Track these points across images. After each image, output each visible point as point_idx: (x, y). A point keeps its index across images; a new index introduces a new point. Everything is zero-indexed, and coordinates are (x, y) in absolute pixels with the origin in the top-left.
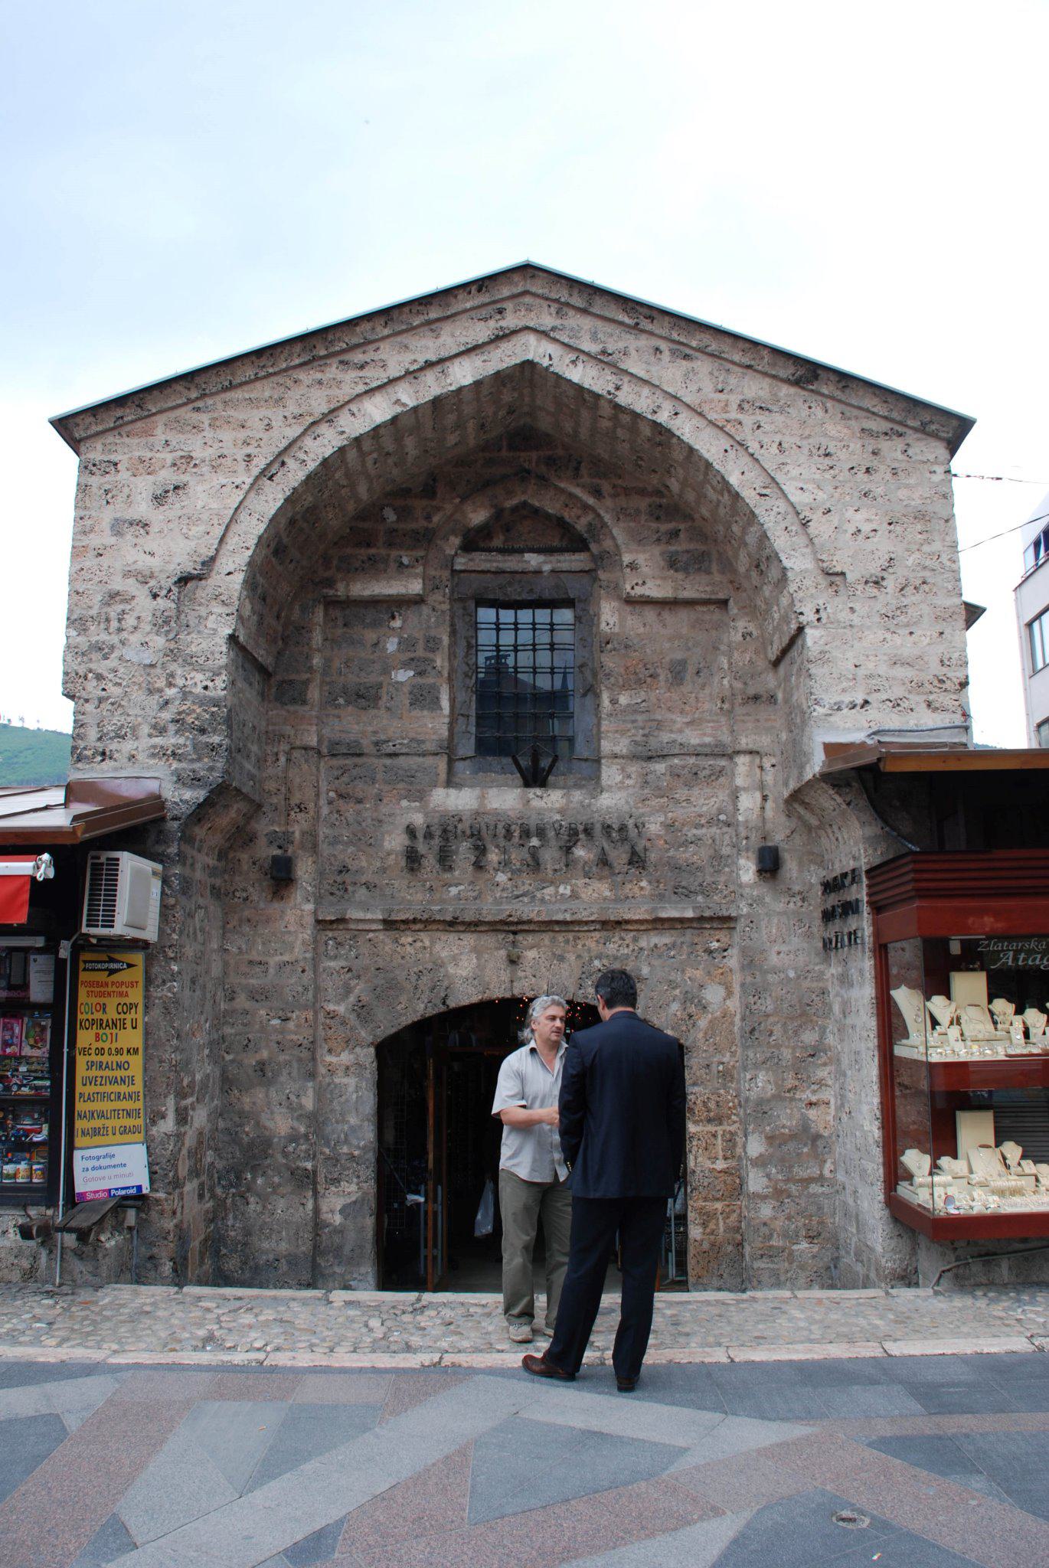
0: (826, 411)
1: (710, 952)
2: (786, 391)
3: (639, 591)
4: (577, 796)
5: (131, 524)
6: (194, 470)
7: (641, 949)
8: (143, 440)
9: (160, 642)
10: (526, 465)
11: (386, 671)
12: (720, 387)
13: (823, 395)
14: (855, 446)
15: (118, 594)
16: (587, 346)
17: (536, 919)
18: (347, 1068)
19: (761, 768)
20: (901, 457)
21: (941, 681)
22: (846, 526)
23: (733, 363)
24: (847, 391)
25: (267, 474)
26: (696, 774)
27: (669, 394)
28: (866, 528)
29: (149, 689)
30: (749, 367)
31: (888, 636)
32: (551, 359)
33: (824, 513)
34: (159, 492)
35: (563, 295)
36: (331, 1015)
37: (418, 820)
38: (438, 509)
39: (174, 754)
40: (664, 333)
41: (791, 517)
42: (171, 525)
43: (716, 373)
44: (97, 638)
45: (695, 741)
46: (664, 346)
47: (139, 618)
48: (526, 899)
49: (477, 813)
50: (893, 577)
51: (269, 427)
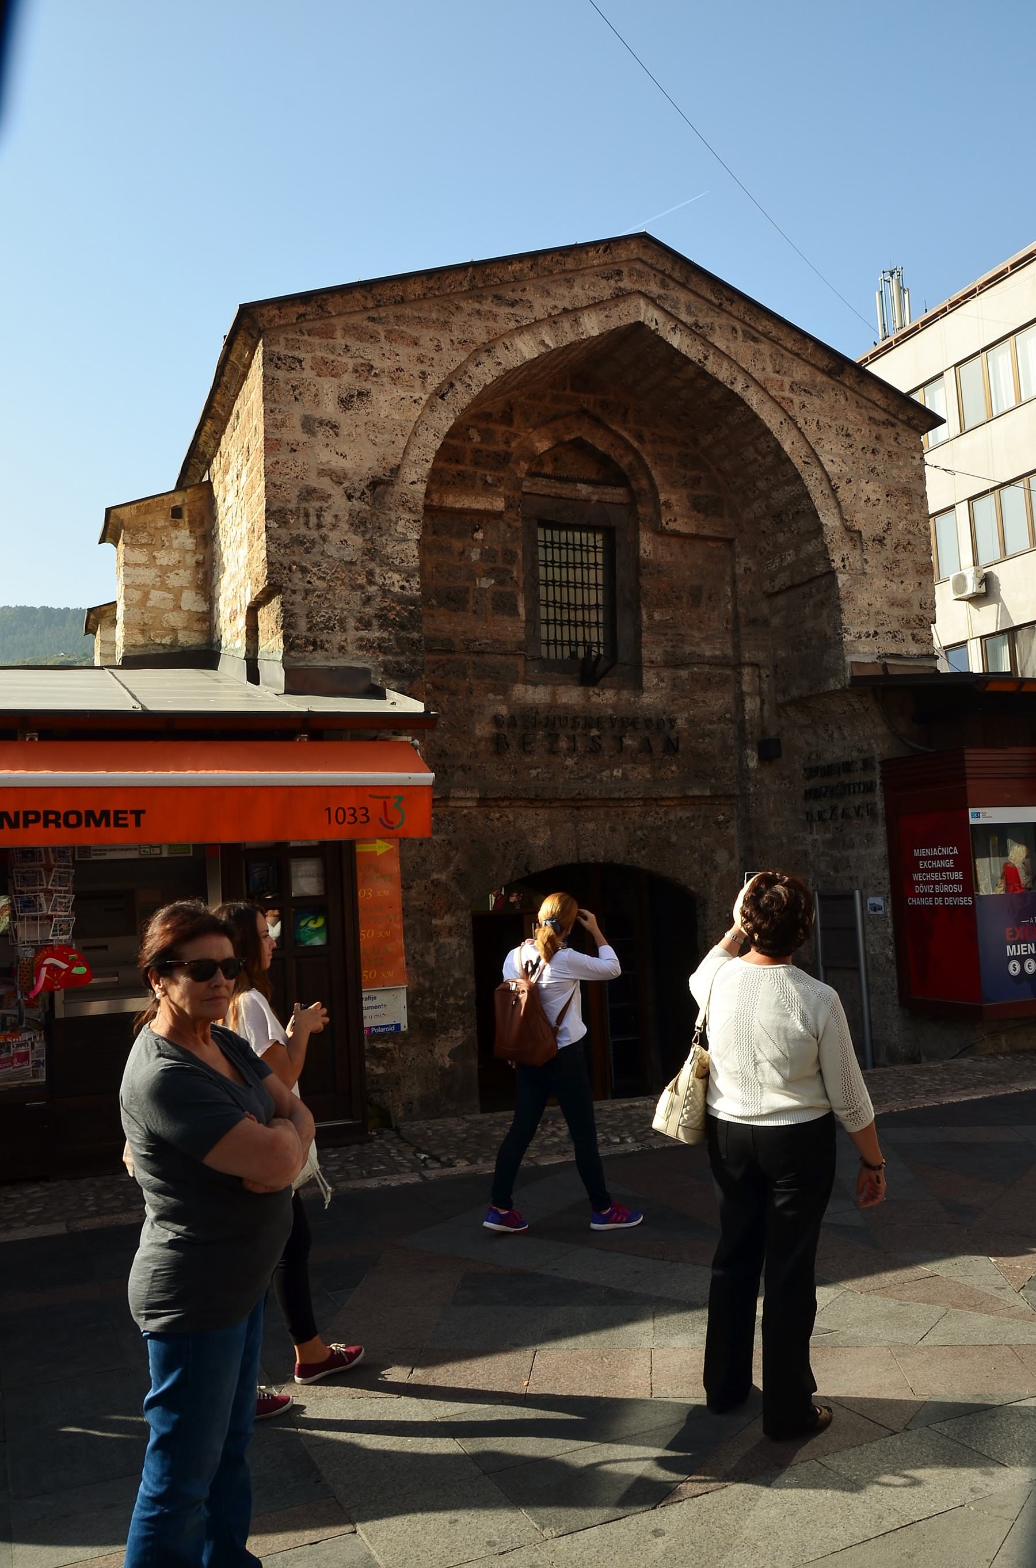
0: (847, 400)
1: (718, 823)
2: (821, 378)
3: (672, 526)
4: (625, 694)
5: (321, 424)
6: (375, 379)
7: (670, 821)
8: (325, 342)
9: (357, 541)
10: (585, 406)
11: (471, 578)
12: (777, 369)
13: (845, 385)
14: (865, 430)
15: (314, 490)
16: (684, 317)
17: (598, 797)
18: (451, 929)
19: (759, 676)
20: (894, 443)
21: (921, 620)
22: (861, 495)
23: (786, 349)
24: (862, 385)
25: (440, 394)
26: (709, 680)
27: (743, 369)
28: (873, 497)
29: (351, 586)
30: (797, 355)
31: (888, 583)
32: (657, 324)
33: (847, 483)
34: (344, 396)
35: (667, 266)
36: (436, 883)
37: (503, 710)
38: (516, 435)
39: (380, 646)
40: (740, 315)
41: (825, 484)
42: (358, 430)
43: (775, 357)
44: (298, 532)
45: (708, 653)
46: (738, 326)
47: (336, 516)
48: (589, 781)
50: (890, 537)
51: (438, 348)
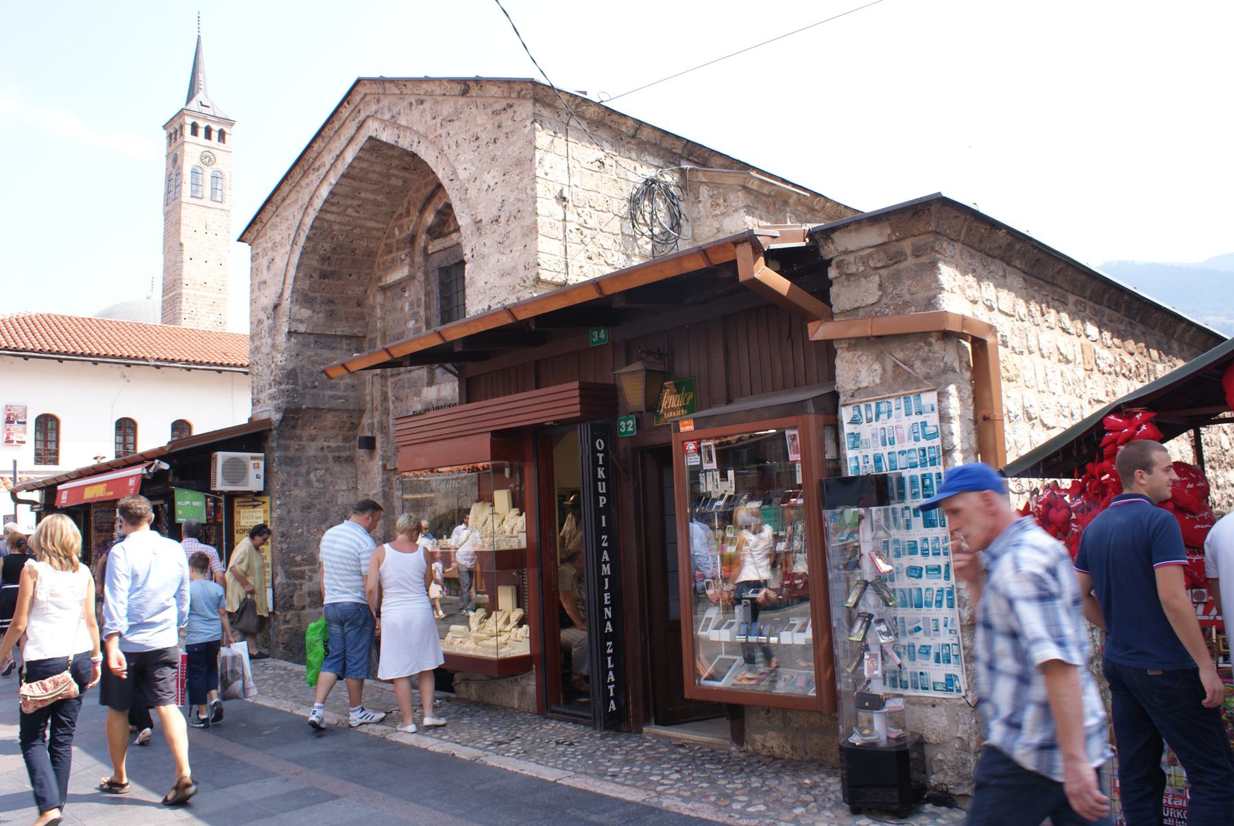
25: (294, 242)
49: (438, 400)
